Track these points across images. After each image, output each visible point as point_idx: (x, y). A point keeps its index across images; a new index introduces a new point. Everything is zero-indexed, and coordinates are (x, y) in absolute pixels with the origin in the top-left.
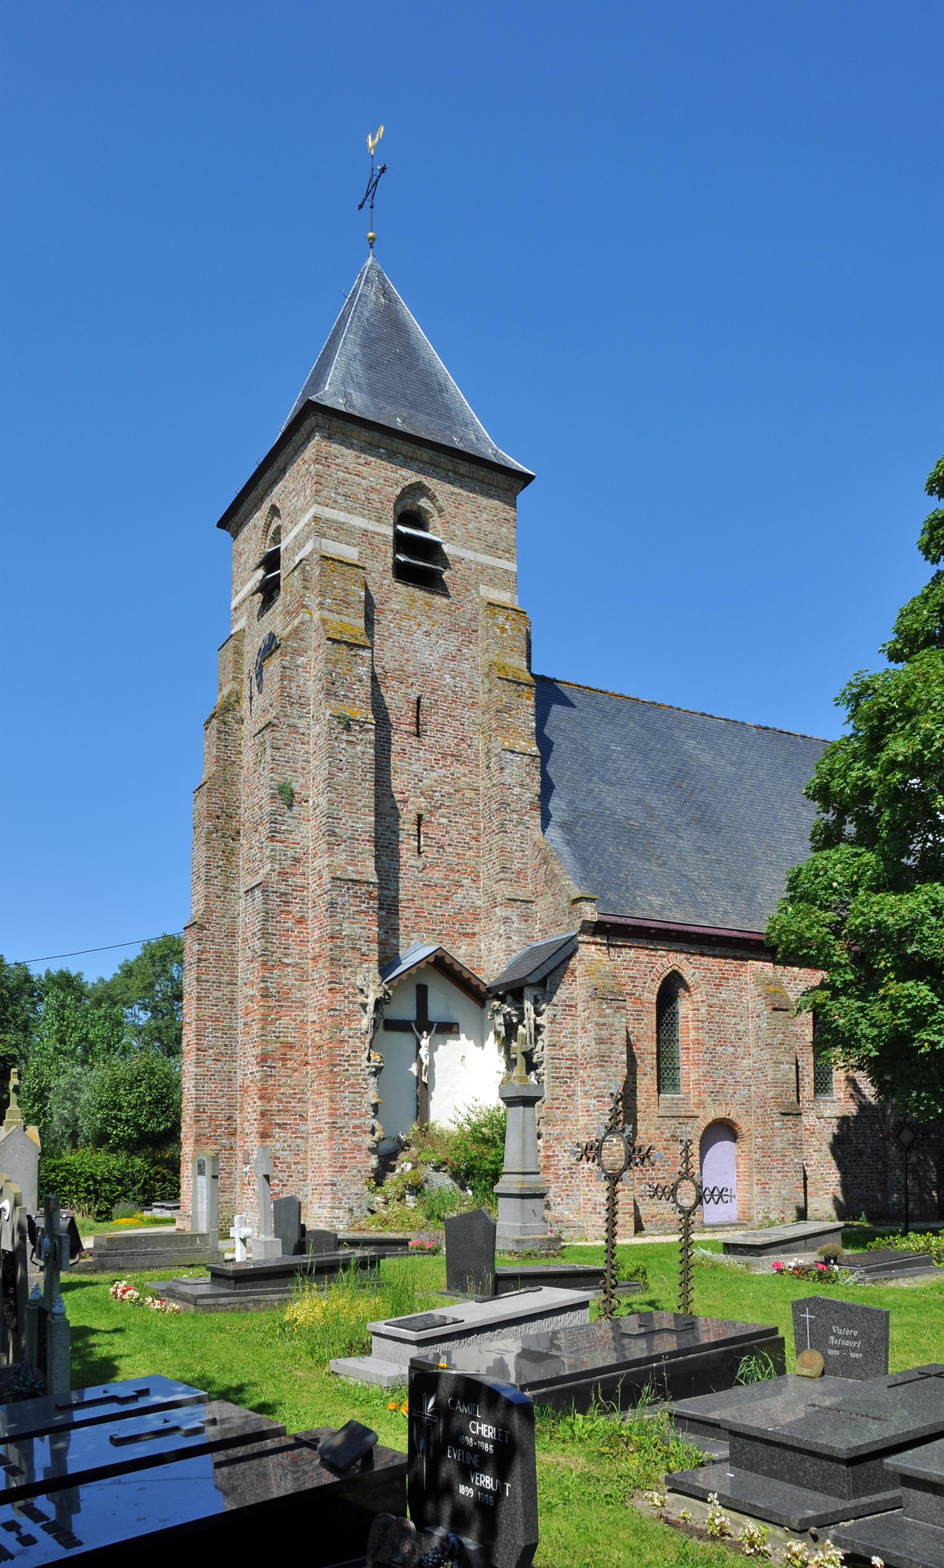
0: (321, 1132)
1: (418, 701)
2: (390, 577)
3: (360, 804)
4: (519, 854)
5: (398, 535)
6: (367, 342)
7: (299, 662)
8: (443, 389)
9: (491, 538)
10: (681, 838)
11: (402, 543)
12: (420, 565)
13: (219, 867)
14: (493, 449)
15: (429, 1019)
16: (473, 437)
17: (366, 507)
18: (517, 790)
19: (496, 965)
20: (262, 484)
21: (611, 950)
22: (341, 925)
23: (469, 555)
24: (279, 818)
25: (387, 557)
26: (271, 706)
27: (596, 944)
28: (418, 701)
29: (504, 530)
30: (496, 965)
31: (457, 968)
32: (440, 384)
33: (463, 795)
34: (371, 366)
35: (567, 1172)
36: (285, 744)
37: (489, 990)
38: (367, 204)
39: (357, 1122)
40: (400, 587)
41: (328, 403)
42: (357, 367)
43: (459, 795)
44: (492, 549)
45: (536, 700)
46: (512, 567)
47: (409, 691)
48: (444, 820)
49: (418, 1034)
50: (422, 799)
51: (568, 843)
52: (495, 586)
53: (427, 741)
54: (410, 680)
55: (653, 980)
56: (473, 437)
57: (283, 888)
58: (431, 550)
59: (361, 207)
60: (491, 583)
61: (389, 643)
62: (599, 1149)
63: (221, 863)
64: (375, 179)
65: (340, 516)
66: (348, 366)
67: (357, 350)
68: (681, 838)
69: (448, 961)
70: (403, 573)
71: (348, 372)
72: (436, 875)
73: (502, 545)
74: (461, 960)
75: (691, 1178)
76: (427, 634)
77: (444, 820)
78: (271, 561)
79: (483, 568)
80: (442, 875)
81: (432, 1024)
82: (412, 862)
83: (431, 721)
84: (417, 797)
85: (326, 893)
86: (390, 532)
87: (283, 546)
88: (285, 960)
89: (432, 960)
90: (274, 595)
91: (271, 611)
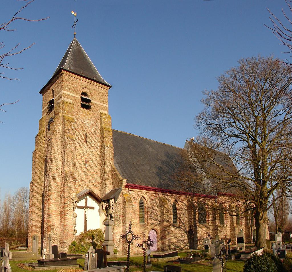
0: (62, 231)
1: (86, 134)
2: (80, 106)
3: (72, 157)
4: (109, 170)
5: (82, 98)
6: (74, 55)
7: (58, 125)
8: (91, 66)
9: (102, 99)
10: (145, 167)
11: (83, 99)
12: (86, 104)
13: (38, 170)
14: (103, 80)
15: (88, 206)
16: (98, 77)
17: (74, 91)
18: (108, 155)
19: (103, 194)
20: (50, 85)
21: (129, 191)
22: (68, 184)
23: (97, 103)
24: (53, 160)
25: (80, 102)
26: (52, 134)
27: (126, 190)
28: (86, 134)
29: (105, 98)
30: (103, 194)
31: (94, 195)
32: (90, 65)
33: (96, 156)
34: (75, 60)
35: (119, 240)
36: (55, 143)
37: (101, 200)
38: (76, 20)
39: (71, 229)
40: (82, 109)
41: (65, 69)
42: (72, 61)
43: (95, 156)
44: (102, 102)
45: (113, 135)
46: (107, 106)
47: (84, 132)
48: (92, 161)
49: (85, 209)
50: (87, 156)
51: (120, 167)
52: (103, 110)
53: (88, 143)
54: (84, 130)
55: (138, 198)
56: (98, 77)
57: (54, 175)
58: (89, 101)
59: (72, 27)
60: (102, 109)
61: (79, 122)
62: (126, 236)
63: (39, 169)
64: (76, 22)
65: (68, 93)
66: (70, 60)
67: (72, 57)
68: (145, 167)
69: (92, 193)
70: (83, 106)
71: (70, 62)
72: (90, 174)
73: (105, 101)
74: (95, 193)
75: (131, 232)
76: (88, 120)
77: (92, 161)
78: (52, 102)
79: (101, 106)
80: (91, 173)
81: (88, 207)
82: (84, 171)
83: (89, 139)
84: (86, 156)
85: (256, 89)
86: (80, 97)
87: (55, 99)
88: (55, 192)
89: (89, 193)
90: (52, 109)
91: (52, 113)
